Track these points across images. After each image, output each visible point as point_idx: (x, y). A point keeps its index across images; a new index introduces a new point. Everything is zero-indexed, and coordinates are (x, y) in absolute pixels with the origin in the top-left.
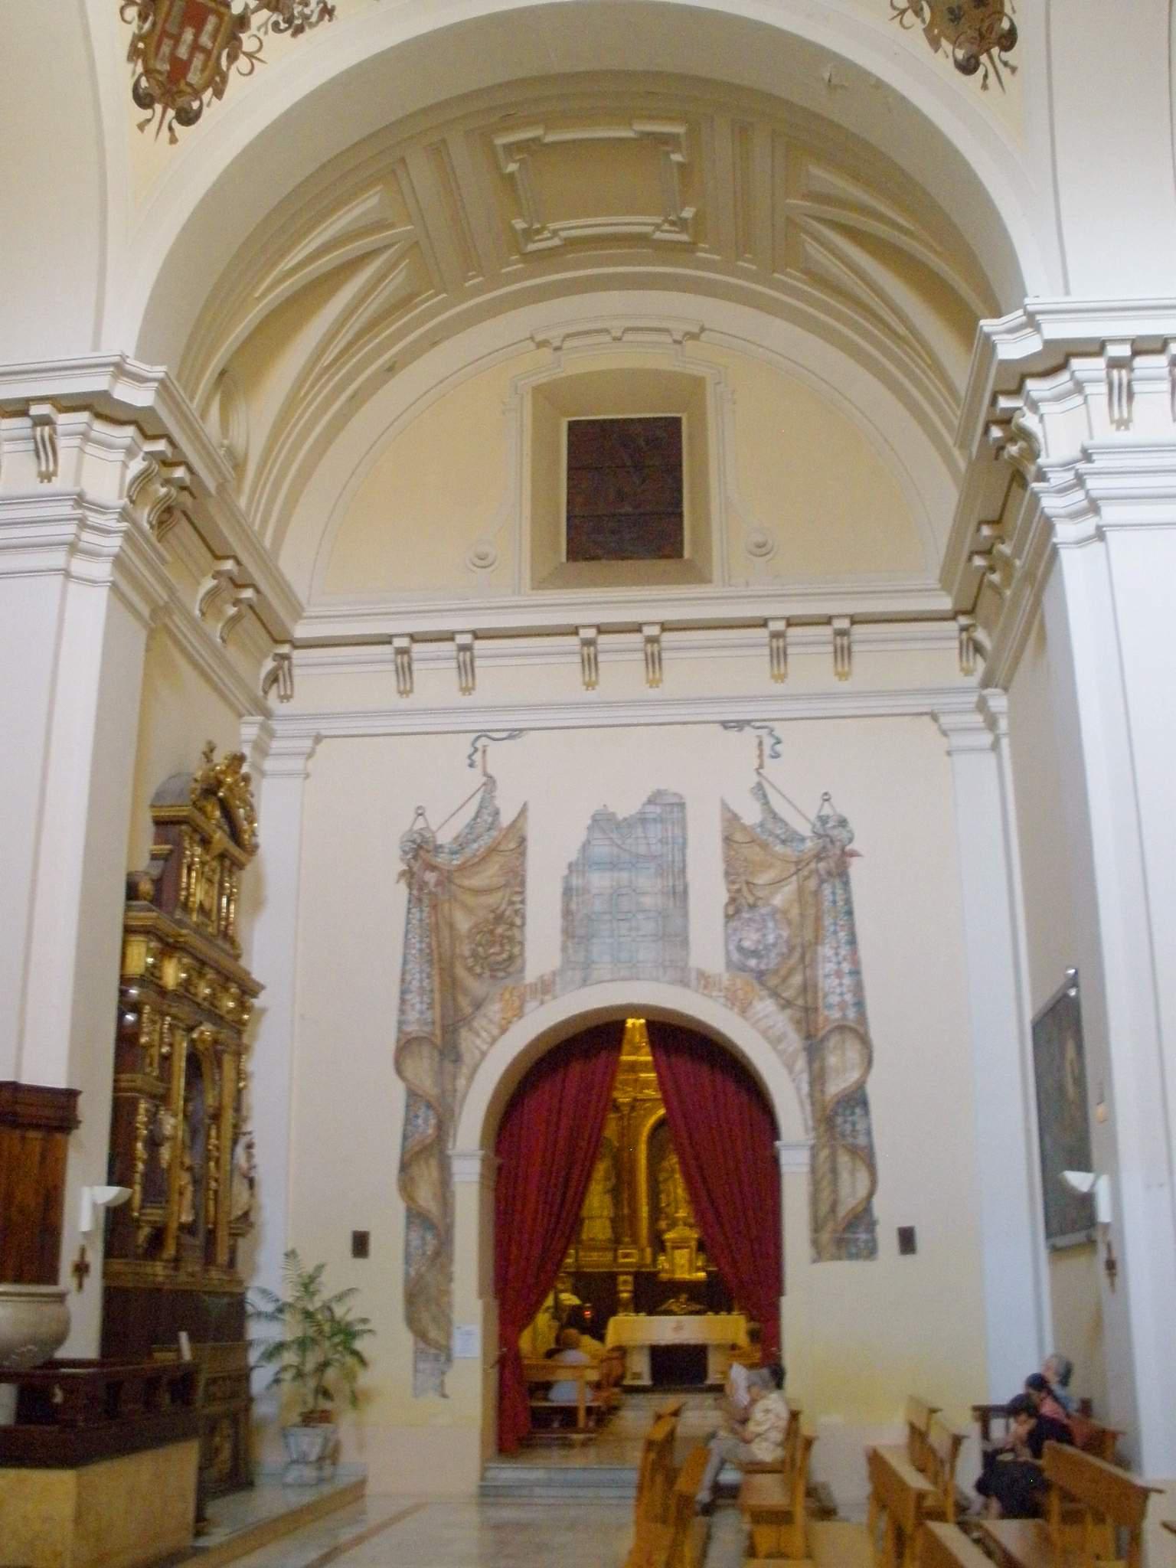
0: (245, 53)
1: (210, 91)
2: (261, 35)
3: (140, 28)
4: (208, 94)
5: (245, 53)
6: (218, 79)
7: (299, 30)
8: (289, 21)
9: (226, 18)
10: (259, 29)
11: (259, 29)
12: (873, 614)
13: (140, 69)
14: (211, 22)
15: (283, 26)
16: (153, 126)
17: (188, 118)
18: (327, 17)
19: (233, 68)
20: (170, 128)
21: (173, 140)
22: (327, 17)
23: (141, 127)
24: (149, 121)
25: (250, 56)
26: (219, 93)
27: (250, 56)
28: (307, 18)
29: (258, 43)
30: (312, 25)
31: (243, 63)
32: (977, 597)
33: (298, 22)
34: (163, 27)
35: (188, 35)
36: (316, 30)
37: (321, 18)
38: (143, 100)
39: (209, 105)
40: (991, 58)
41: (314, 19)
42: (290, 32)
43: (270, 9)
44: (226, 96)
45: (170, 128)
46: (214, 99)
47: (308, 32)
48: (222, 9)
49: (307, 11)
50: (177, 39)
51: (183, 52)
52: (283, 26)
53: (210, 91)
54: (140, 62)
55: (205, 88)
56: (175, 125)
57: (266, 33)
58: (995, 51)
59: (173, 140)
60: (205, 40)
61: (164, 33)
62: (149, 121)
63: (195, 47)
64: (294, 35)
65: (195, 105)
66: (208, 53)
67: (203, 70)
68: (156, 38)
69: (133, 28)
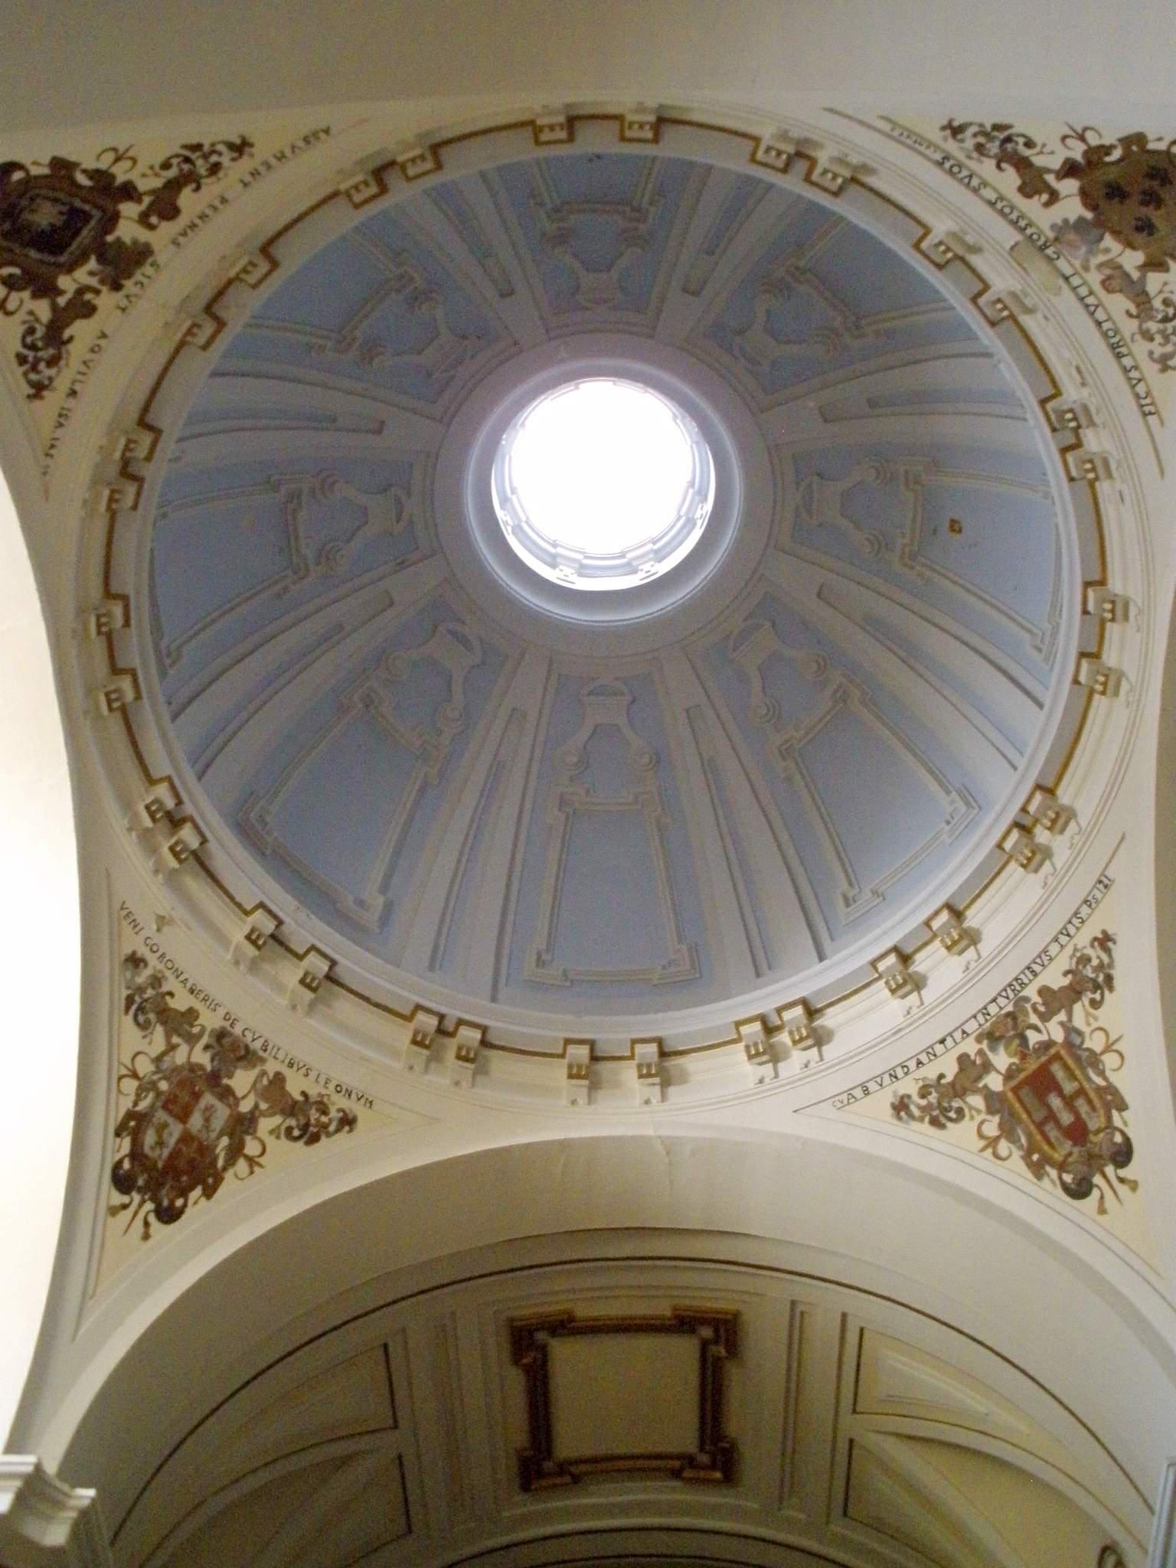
0: (1102, 1053)
1: (1115, 1113)
2: (1095, 1025)
3: (1021, 1147)
4: (1117, 1118)
5: (1102, 1053)
6: (1109, 1097)
7: (1109, 979)
8: (1097, 987)
9: (1063, 1052)
10: (1089, 1025)
11: (1089, 1025)
12: (106, 657)
13: (1053, 1173)
14: (1057, 1070)
15: (1097, 996)
16: (1110, 1199)
17: (1123, 1155)
18: (1110, 944)
19: (1108, 1073)
20: (1122, 1180)
21: (1134, 1186)
22: (1110, 944)
23: (1102, 1210)
24: (1102, 1197)
25: (1108, 1049)
26: (1122, 1107)
27: (1108, 1049)
28: (1101, 967)
29: (1101, 1034)
30: (1111, 965)
31: (1110, 1061)
32: (231, 898)
33: (1101, 978)
34: (1033, 1122)
35: (1055, 1102)
36: (1118, 962)
37: (1108, 951)
38: (1079, 1191)
39: (1125, 1123)
40: (1105, 1176)
41: (1106, 959)
42: (1107, 992)
43: (1075, 1002)
44: (1128, 1098)
45: (1122, 1180)
46: (1124, 1114)
47: (1117, 973)
48: (1053, 1051)
49: (1095, 962)
50: (1052, 1116)
51: (1066, 1118)
52: (1097, 996)
53: (1115, 1113)
54: (1048, 1168)
55: (1109, 1118)
56: (1122, 1173)
57: (1096, 1019)
58: (1110, 1170)
59: (1134, 1186)
60: (1069, 1087)
61: (1040, 1126)
62: (1102, 1197)
63: (1069, 1102)
64: (1111, 989)
65: (1118, 1138)
66: (1081, 1092)
67: (1094, 1109)
68: (1039, 1137)
69: (1017, 1154)
